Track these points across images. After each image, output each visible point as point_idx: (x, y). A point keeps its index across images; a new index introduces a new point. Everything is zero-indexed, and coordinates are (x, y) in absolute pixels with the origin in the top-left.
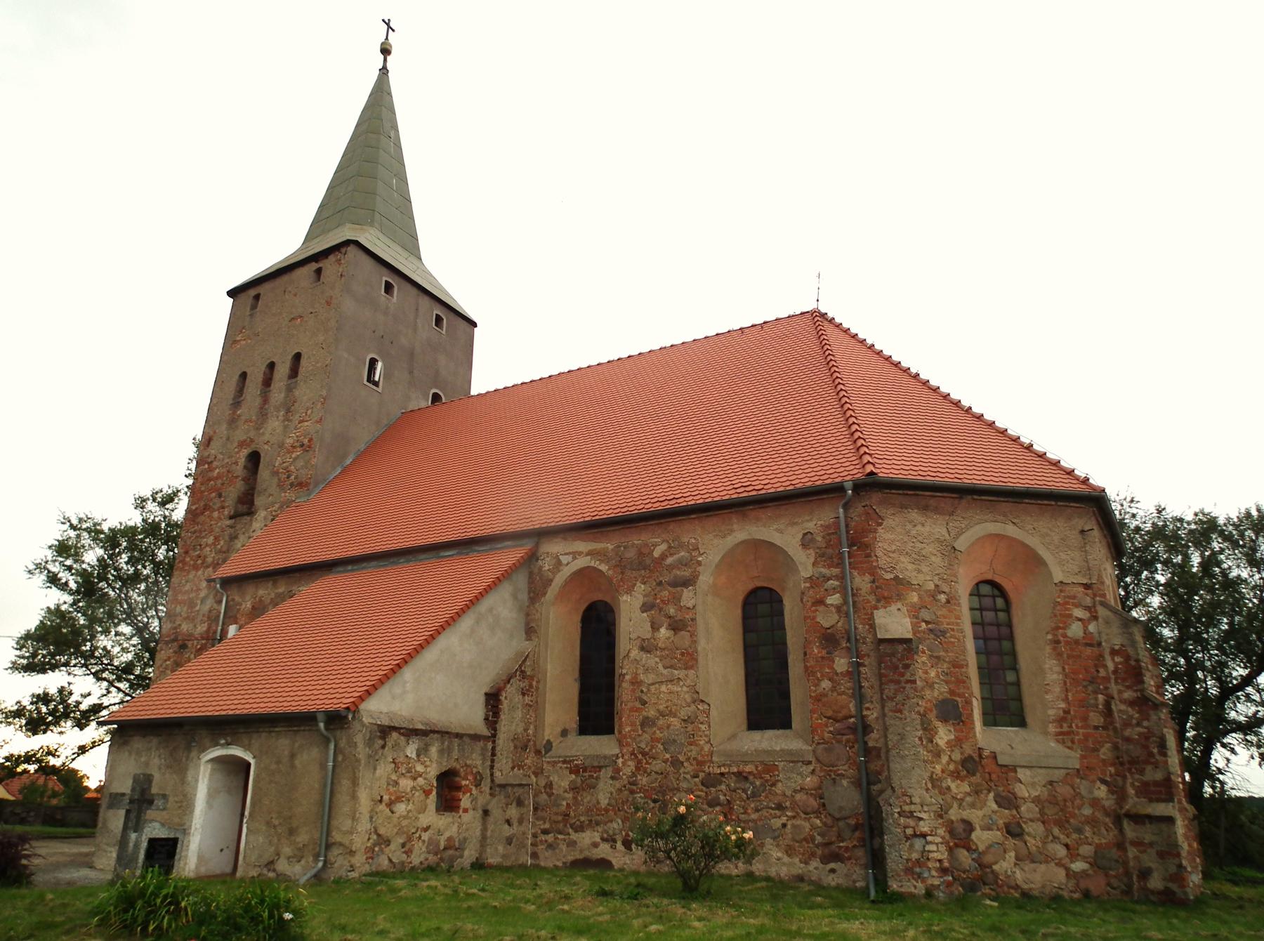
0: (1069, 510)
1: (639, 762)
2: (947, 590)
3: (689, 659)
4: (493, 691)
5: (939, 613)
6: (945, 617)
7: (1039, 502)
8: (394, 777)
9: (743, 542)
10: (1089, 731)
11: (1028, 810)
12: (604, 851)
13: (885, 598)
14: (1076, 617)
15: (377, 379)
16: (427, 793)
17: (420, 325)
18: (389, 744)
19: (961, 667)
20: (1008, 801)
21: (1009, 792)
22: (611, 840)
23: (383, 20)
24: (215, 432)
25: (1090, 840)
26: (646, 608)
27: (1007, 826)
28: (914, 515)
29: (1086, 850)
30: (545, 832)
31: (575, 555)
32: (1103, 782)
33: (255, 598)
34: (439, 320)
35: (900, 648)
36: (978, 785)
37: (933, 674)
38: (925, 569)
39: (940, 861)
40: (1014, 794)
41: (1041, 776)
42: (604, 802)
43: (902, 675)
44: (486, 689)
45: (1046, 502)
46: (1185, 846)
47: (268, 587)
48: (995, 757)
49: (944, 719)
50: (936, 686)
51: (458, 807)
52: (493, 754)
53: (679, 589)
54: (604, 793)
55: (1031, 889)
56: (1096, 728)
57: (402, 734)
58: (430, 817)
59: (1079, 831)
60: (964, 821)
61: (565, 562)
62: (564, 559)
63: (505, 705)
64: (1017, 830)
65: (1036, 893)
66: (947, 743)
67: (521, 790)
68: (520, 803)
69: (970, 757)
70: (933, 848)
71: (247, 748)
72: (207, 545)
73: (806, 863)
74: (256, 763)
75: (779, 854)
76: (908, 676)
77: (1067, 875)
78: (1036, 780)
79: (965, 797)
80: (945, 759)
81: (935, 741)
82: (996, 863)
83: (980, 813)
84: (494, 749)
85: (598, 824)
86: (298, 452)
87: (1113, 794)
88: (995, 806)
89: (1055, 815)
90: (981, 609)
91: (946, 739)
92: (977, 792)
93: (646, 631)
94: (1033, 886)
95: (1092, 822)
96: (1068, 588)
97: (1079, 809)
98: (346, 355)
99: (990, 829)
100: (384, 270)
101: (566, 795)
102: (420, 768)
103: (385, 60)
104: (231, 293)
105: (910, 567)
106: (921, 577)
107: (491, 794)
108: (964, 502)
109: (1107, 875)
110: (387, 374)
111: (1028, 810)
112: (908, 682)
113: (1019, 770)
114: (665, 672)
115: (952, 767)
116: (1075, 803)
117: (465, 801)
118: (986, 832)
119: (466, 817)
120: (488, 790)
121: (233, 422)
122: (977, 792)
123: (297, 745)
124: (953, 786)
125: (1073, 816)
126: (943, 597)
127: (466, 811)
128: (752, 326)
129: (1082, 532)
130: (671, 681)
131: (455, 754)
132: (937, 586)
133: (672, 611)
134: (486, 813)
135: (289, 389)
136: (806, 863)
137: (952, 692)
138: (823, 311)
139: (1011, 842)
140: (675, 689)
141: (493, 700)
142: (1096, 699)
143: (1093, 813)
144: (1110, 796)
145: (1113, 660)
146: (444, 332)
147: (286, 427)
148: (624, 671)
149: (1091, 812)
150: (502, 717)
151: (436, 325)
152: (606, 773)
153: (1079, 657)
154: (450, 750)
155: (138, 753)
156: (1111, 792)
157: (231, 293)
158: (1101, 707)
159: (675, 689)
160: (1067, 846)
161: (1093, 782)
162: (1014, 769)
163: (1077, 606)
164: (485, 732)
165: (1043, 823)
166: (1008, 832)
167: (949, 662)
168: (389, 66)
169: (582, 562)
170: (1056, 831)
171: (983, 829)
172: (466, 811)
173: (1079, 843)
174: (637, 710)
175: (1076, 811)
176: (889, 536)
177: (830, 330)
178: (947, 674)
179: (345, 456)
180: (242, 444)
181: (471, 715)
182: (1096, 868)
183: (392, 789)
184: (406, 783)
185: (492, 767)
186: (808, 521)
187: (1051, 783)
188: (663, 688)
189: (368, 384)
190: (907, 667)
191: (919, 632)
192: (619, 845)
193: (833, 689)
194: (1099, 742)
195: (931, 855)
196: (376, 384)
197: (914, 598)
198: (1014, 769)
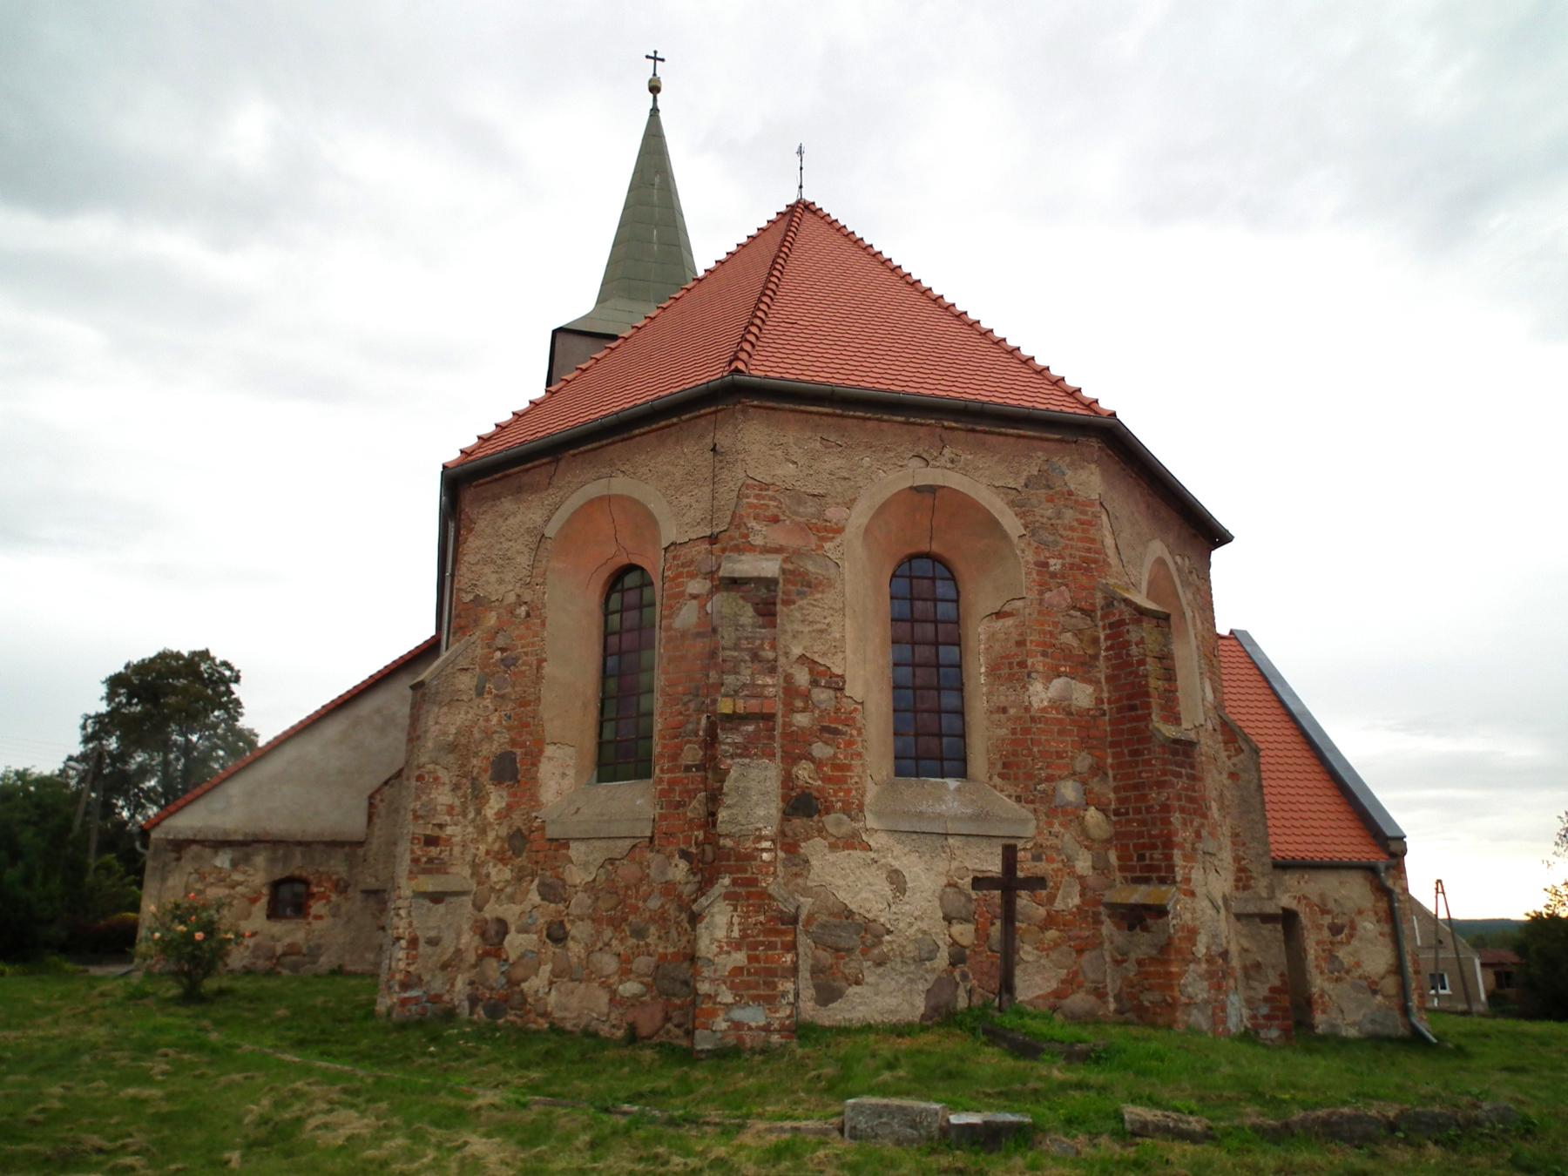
0: (703, 422)
7: (654, 426)
10: (678, 775)
14: (690, 595)
16: (253, 901)
21: (557, 877)
23: (647, 57)
25: (652, 948)
27: (550, 925)
28: (507, 505)
29: (643, 963)
32: (685, 855)
36: (521, 869)
37: (494, 720)
40: (563, 880)
41: (599, 851)
45: (663, 423)
49: (498, 779)
50: (496, 736)
51: (309, 914)
55: (564, 1019)
56: (688, 768)
59: (639, 933)
64: (559, 933)
65: (568, 1026)
66: (496, 814)
77: (611, 1000)
78: (591, 858)
79: (505, 887)
81: (483, 812)
82: (525, 980)
83: (517, 909)
87: (695, 874)
89: (614, 908)
90: (641, 607)
92: (520, 879)
94: (567, 1014)
96: (683, 551)
97: (645, 901)
99: (527, 932)
102: (237, 877)
106: (502, 589)
108: (562, 464)
111: (580, 902)
113: (572, 844)
115: (496, 847)
116: (641, 890)
118: (521, 936)
124: (493, 872)
125: (635, 909)
126: (522, 610)
132: (518, 596)
137: (513, 742)
139: (551, 948)
143: (662, 906)
144: (691, 877)
149: (659, 904)
156: (692, 871)
158: (701, 733)
161: (670, 856)
163: (692, 576)
167: (514, 701)
168: (659, 105)
171: (520, 931)
175: (640, 904)
176: (478, 543)
178: (510, 717)
187: (611, 861)
194: (688, 792)
197: (491, 620)
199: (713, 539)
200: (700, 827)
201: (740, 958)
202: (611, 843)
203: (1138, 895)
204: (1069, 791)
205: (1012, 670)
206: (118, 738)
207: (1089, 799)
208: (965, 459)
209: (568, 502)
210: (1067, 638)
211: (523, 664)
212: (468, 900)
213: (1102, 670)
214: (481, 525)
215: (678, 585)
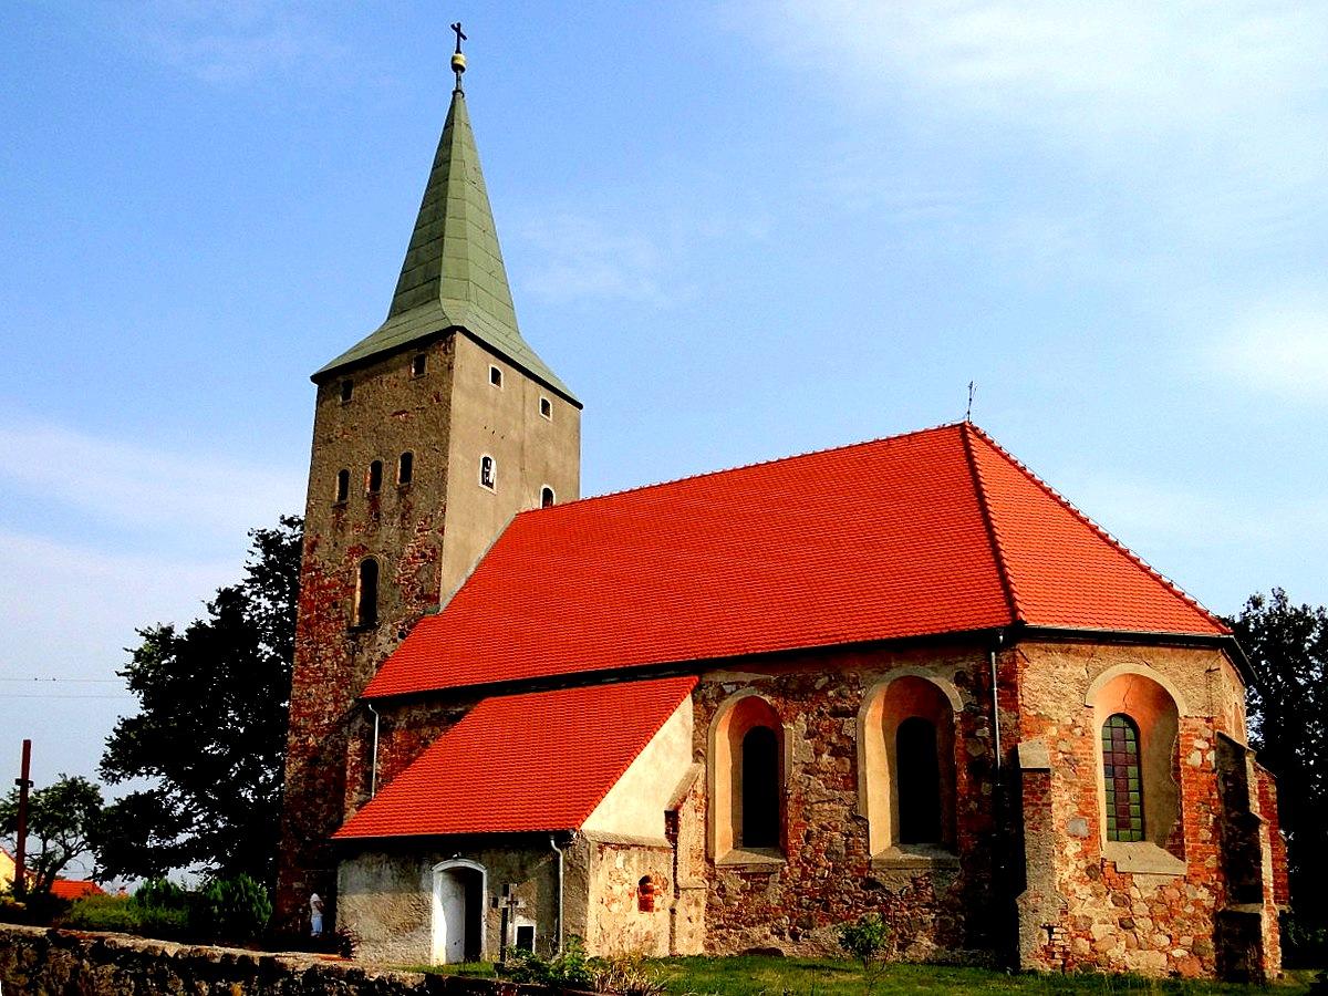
1: (805, 869)
2: (1083, 724)
4: (671, 810)
5: (1074, 745)
6: (1079, 748)
9: (901, 678)
12: (774, 941)
13: (1028, 732)
17: (527, 414)
18: (605, 857)
19: (1091, 790)
20: (1123, 901)
22: (781, 934)
24: (318, 536)
26: (810, 735)
28: (1059, 658)
29: (1187, 940)
30: (721, 927)
31: (739, 684)
32: (1206, 886)
33: (409, 718)
34: (496, 376)
35: (1039, 776)
39: (1064, 947)
41: (1153, 882)
42: (774, 903)
43: (1040, 799)
44: (665, 807)
46: (1269, 938)
47: (422, 708)
48: (1115, 867)
52: (675, 863)
53: (840, 719)
54: (774, 894)
56: (1204, 842)
57: (614, 848)
58: (635, 914)
61: (728, 691)
62: (728, 689)
63: (682, 822)
64: (1129, 924)
69: (1094, 865)
70: (1059, 937)
71: (479, 860)
72: (327, 658)
73: (952, 950)
74: (488, 873)
75: (929, 943)
76: (1045, 800)
80: (1072, 867)
84: (675, 858)
85: (767, 920)
86: (421, 563)
88: (1112, 906)
91: (1074, 851)
93: (809, 757)
95: (1193, 917)
98: (461, 457)
99: (1106, 923)
100: (491, 357)
101: (738, 897)
102: (626, 876)
103: (458, 79)
104: (315, 379)
105: (1051, 704)
106: (1060, 713)
107: (675, 897)
109: (1201, 959)
110: (500, 474)
111: (1140, 909)
112: (1044, 805)
114: (827, 792)
115: (1077, 874)
117: (657, 902)
119: (659, 915)
120: (673, 894)
121: (339, 526)
123: (525, 858)
124: (1077, 889)
126: (1078, 731)
127: (658, 910)
128: (898, 437)
129: (1209, 671)
130: (832, 800)
131: (649, 864)
133: (834, 739)
134: (673, 911)
135: (402, 493)
136: (952, 950)
138: (975, 425)
140: (836, 807)
141: (672, 817)
142: (1207, 817)
145: (1225, 784)
146: (550, 419)
147: (402, 536)
148: (789, 791)
150: (681, 831)
151: (493, 381)
153: (1196, 781)
154: (645, 860)
155: (369, 866)
156: (1211, 894)
157: (315, 379)
159: (836, 807)
160: (1170, 936)
161: (1197, 887)
162: (1131, 875)
164: (669, 845)
165: (1152, 919)
166: (1122, 926)
168: (470, 109)
169: (744, 693)
170: (1162, 925)
172: (658, 910)
173: (1180, 934)
174: (803, 825)
177: (981, 454)
179: (468, 567)
180: (353, 551)
181: (656, 830)
182: (1192, 955)
184: (617, 889)
185: (675, 874)
186: (961, 661)
187: (1161, 887)
188: (826, 806)
189: (484, 486)
190: (1044, 792)
191: (1056, 761)
192: (787, 937)
193: (979, 809)
195: (1056, 942)
196: (491, 485)
197: (1053, 731)
198: (1131, 875)
200: (1215, 872)
202: (1161, 878)
206: (48, 931)
208: (304, 613)
209: (1108, 671)
211: (1084, 765)
215: (1188, 740)
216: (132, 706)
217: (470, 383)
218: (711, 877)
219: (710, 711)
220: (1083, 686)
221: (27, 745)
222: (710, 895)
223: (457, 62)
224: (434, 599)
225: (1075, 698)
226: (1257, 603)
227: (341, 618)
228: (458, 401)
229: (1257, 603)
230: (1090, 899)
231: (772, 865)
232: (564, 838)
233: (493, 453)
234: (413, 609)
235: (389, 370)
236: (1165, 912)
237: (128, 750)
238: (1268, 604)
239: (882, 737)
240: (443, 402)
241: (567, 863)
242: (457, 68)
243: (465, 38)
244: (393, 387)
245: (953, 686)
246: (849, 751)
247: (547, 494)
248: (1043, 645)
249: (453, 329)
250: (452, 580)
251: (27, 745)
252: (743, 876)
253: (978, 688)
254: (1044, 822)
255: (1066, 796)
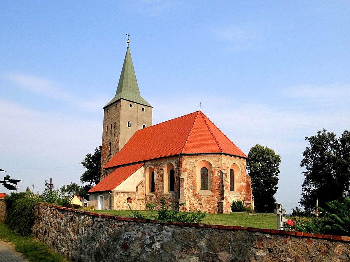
3: (162, 181)
8: (120, 198)
11: (203, 201)
15: (130, 126)
26: (158, 173)
28: (190, 158)
32: (216, 197)
34: (143, 109)
38: (191, 167)
41: (206, 197)
60: (193, 203)
63: (139, 188)
67: (142, 200)
68: (142, 202)
71: (103, 195)
80: (191, 194)
88: (198, 201)
98: (123, 123)
99: (197, 204)
103: (128, 45)
104: (103, 108)
105: (188, 167)
106: (190, 168)
115: (192, 196)
122: (195, 199)
126: (193, 171)
131: (130, 195)
135: (114, 130)
151: (130, 107)
152: (153, 197)
157: (103, 108)
168: (131, 50)
170: (207, 204)
181: (135, 190)
183: (119, 200)
197: (188, 171)
199: (219, 168)
201: (226, 206)
203: (248, 202)
204: (243, 193)
205: (239, 181)
207: (244, 194)
210: (243, 179)
212: (188, 201)
213: (245, 182)
214: (185, 160)
216: (85, 170)
217: (124, 108)
218: (146, 198)
219: (146, 169)
220: (194, 163)
221: (51, 179)
222: (145, 201)
223: (128, 42)
224: (118, 149)
225: (193, 165)
226: (319, 132)
227: (107, 153)
228: (122, 112)
229: (319, 132)
230: (194, 200)
231: (153, 195)
232: (111, 192)
233: (130, 120)
234: (116, 151)
235: (112, 107)
236: (208, 201)
237: (85, 178)
238: (322, 132)
239: (167, 173)
240: (119, 112)
241: (112, 195)
242: (128, 43)
243: (129, 36)
244: (113, 109)
245: (175, 164)
246: (162, 176)
247: (144, 126)
248: (187, 156)
249: (121, 99)
250: (121, 146)
251: (51, 179)
252: (149, 197)
253: (177, 164)
254: (183, 186)
255: (190, 182)
